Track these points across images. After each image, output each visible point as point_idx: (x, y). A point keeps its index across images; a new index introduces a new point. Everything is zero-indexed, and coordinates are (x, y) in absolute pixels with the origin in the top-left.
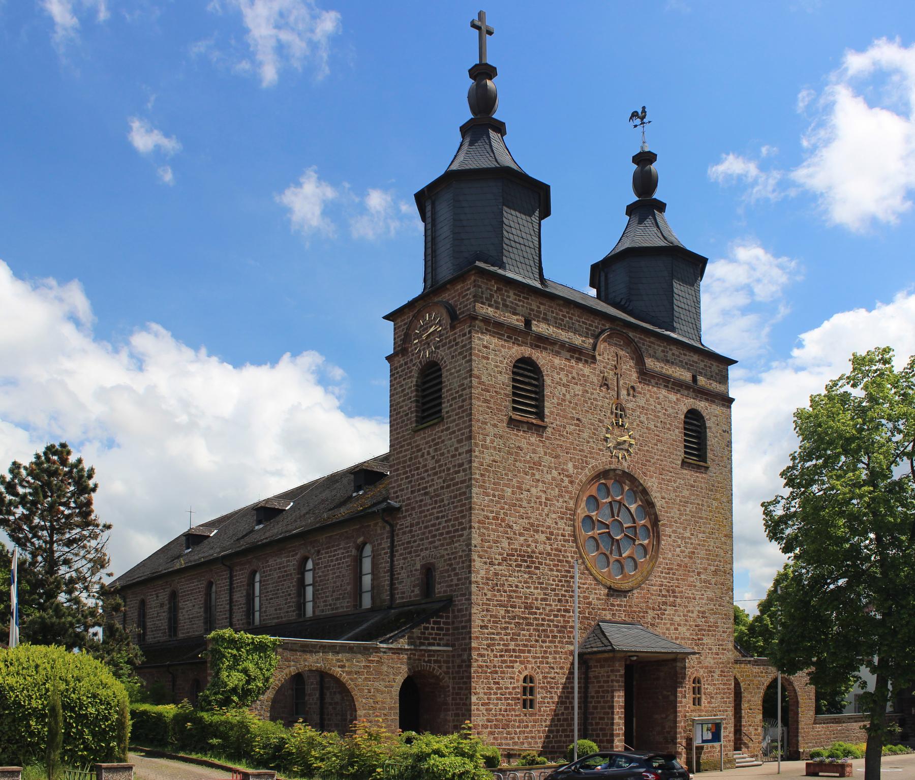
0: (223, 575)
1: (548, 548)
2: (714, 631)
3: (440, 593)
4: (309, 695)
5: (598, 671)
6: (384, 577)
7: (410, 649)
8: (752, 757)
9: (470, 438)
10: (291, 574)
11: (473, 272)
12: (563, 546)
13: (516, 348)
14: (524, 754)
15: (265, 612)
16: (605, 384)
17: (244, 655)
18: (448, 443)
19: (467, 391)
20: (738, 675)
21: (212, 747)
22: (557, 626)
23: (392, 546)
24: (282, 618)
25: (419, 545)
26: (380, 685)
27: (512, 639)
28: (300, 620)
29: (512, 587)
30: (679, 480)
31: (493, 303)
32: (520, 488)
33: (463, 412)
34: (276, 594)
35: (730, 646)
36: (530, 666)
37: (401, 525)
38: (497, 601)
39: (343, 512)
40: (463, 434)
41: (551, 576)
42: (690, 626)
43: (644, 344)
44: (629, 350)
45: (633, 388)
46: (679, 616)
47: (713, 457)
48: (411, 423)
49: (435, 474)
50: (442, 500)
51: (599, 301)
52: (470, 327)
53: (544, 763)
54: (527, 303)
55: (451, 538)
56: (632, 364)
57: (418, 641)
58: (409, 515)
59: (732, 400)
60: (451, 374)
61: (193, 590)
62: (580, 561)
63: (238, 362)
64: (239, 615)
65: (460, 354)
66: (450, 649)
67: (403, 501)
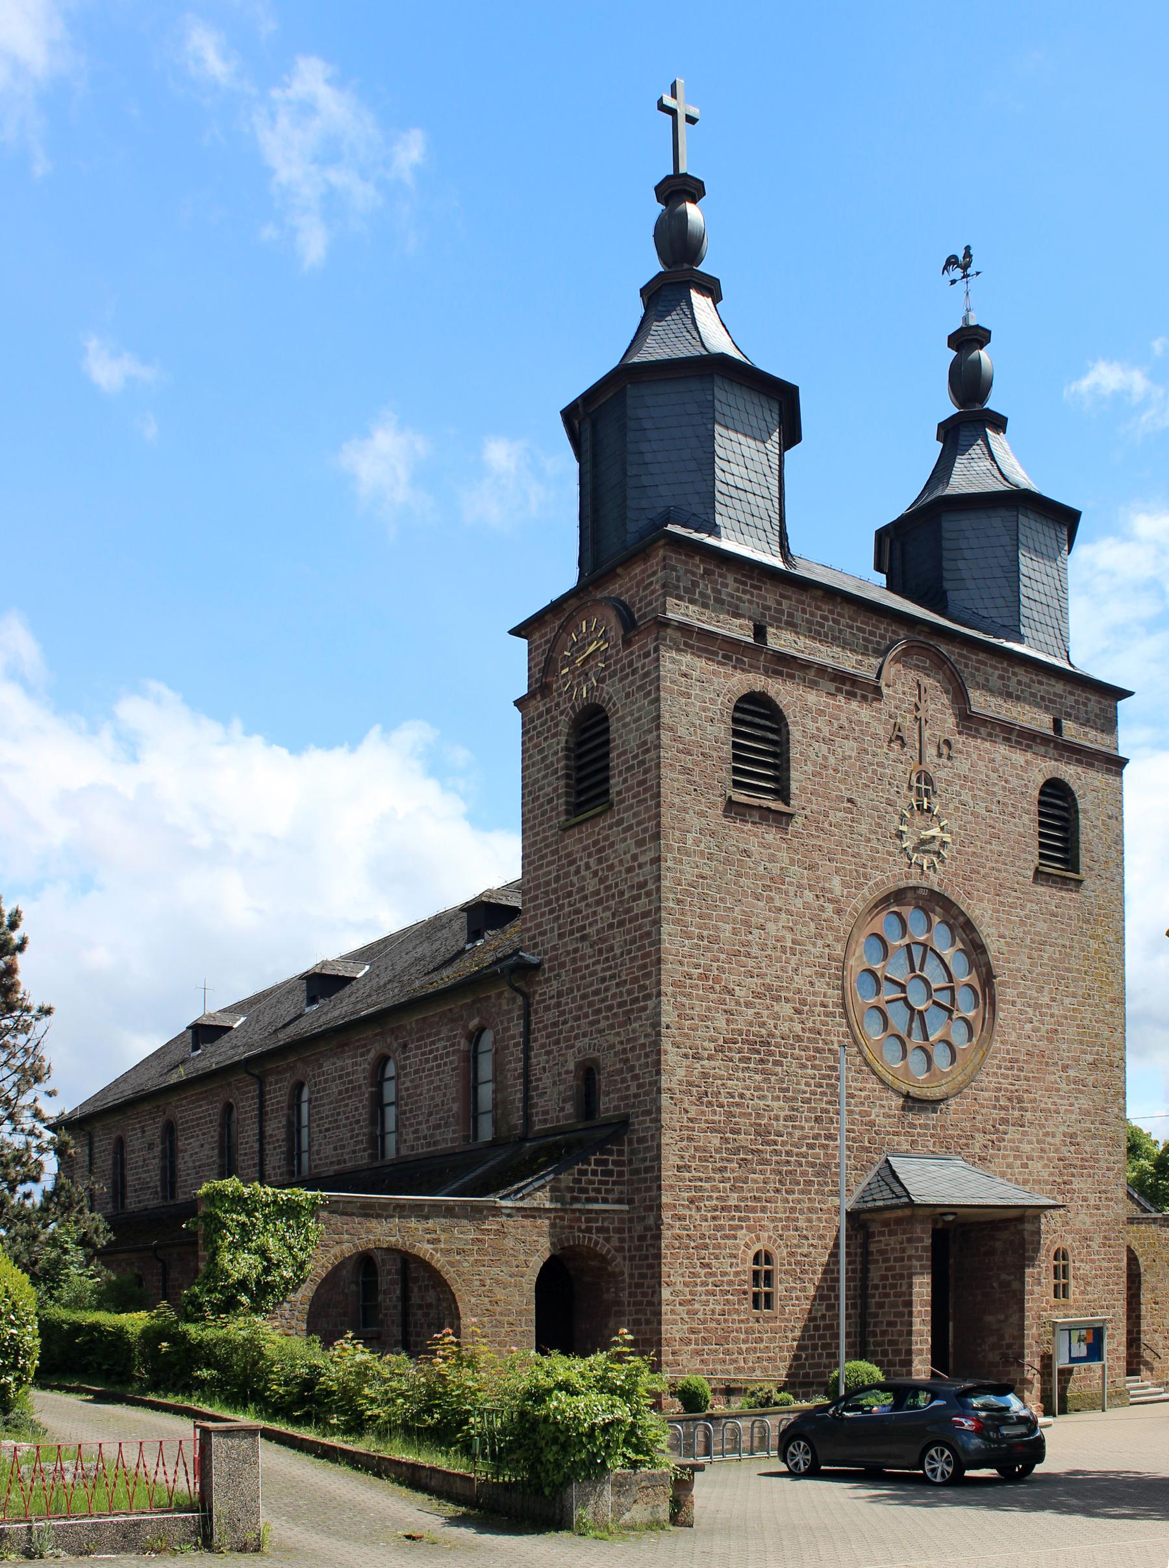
0: (249, 1092)
1: (798, 1028)
2: (1092, 1167)
3: (607, 1110)
4: (385, 1292)
5: (883, 1242)
6: (514, 1086)
7: (555, 1210)
9: (657, 836)
10: (360, 1086)
11: (662, 542)
12: (825, 1024)
13: (739, 675)
14: (752, 1388)
15: (318, 1152)
16: (898, 738)
17: (260, 1224)
18: (621, 847)
19: (653, 754)
20: (1135, 1245)
21: (201, 1383)
22: (813, 1165)
23: (527, 1032)
24: (345, 1162)
25: (572, 1029)
26: (500, 1272)
27: (733, 1189)
28: (376, 1164)
29: (733, 1097)
30: (1029, 905)
31: (697, 597)
32: (746, 923)
33: (646, 791)
34: (336, 1121)
35: (1121, 1193)
36: (766, 1235)
37: (541, 995)
38: (707, 1121)
39: (449, 975)
40: (645, 830)
41: (803, 1080)
42: (1049, 1159)
43: (966, 666)
44: (940, 677)
45: (947, 743)
46: (1030, 1142)
47: (1091, 863)
48: (558, 815)
49: (599, 902)
50: (611, 949)
51: (888, 593)
52: (657, 639)
54: (759, 596)
56: (946, 702)
57: (568, 1196)
58: (555, 976)
59: (1122, 763)
60: (625, 726)
61: (201, 1118)
63: (296, 748)
64: (275, 1160)
65: (640, 688)
66: (626, 1207)
67: (546, 953)
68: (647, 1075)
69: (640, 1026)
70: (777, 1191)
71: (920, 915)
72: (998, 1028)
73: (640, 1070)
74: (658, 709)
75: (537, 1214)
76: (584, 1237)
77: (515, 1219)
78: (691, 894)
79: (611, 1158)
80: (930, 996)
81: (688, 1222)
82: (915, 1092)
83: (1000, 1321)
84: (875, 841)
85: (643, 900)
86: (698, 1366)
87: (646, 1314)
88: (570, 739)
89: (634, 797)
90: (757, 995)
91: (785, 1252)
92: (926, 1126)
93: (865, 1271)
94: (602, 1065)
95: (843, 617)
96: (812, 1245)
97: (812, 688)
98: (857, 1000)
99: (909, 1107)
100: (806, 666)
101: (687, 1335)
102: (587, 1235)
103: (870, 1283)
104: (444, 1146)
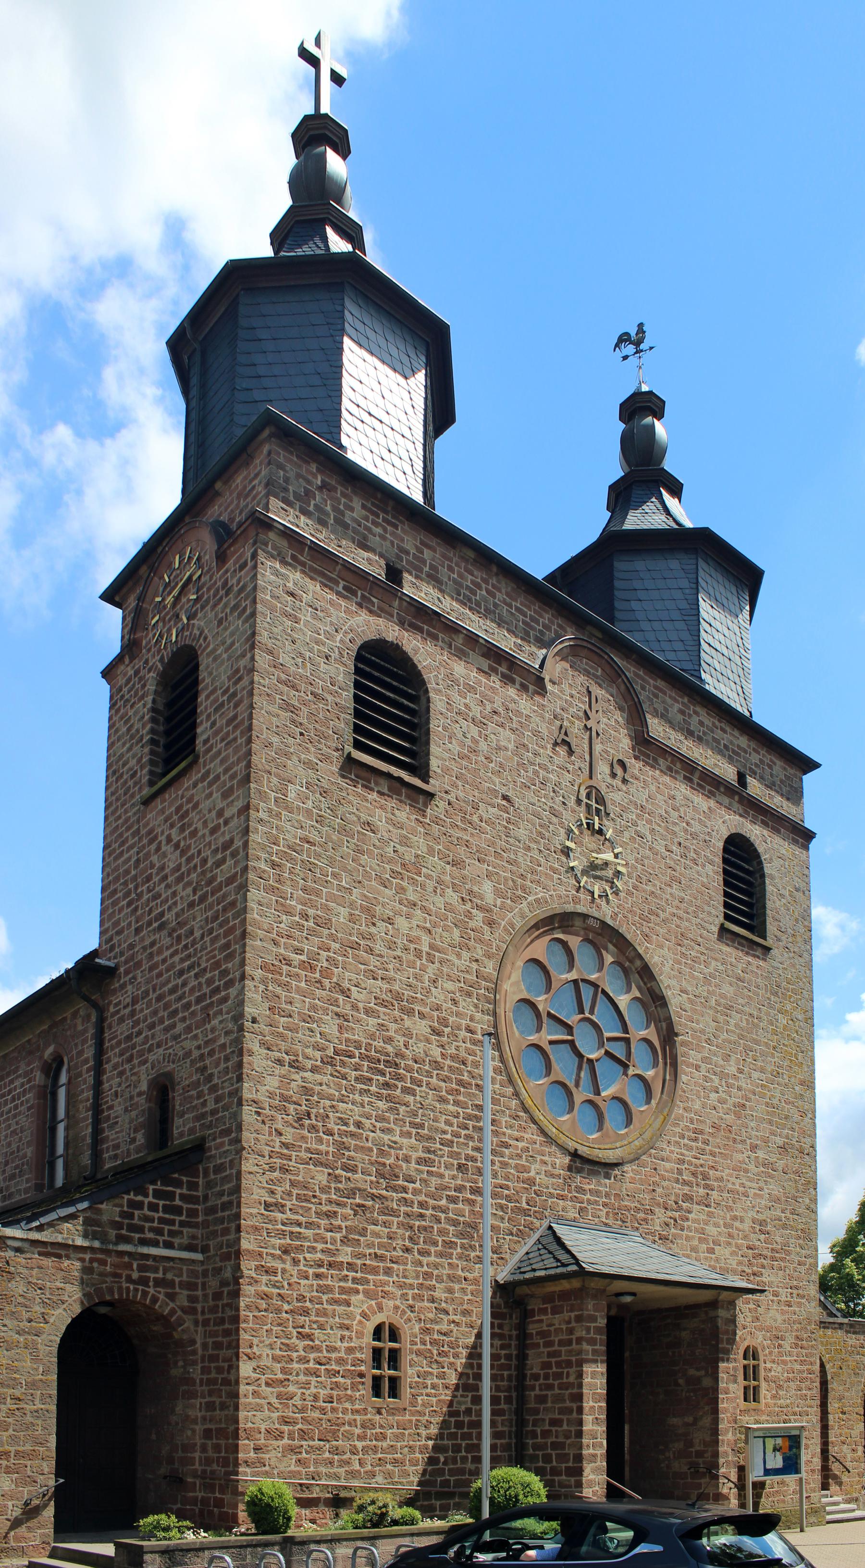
1: (436, 1052)
3: (181, 1135)
7: (91, 1249)
8: (848, 1501)
9: (247, 779)
11: (266, 433)
22: (455, 1223)
27: (345, 1241)
29: (346, 1124)
30: (713, 963)
31: (311, 508)
32: (367, 910)
36: (391, 1303)
37: (116, 1005)
38: (308, 1150)
42: (737, 1246)
44: (614, 691)
45: (621, 763)
46: (716, 1225)
47: (779, 934)
49: (180, 879)
50: (191, 932)
53: (413, 1522)
54: (392, 534)
55: (205, 1009)
57: (112, 1233)
62: (510, 1090)
66: (199, 1257)
67: (122, 954)
68: (226, 1084)
69: (221, 1022)
70: (407, 1250)
71: (589, 950)
72: (680, 1093)
73: (219, 1078)
74: (254, 625)
75: (63, 1253)
76: (136, 1290)
77: (28, 1255)
78: (291, 859)
79: (178, 1191)
80: (601, 1044)
81: (279, 1278)
82: (583, 1151)
83: (687, 1424)
84: (537, 852)
85: (228, 863)
86: (293, 1468)
87: (221, 1397)
88: (159, 699)
89: (222, 740)
90: (383, 1004)
91: (417, 1327)
92: (597, 1193)
93: (522, 1357)
94: (177, 1079)
95: (500, 591)
96: (454, 1322)
97: (460, 659)
98: (513, 1033)
99: (576, 1168)
100: (453, 629)
101: (277, 1426)
102: (140, 1287)
103: (529, 1372)
104: (17, 1198)
